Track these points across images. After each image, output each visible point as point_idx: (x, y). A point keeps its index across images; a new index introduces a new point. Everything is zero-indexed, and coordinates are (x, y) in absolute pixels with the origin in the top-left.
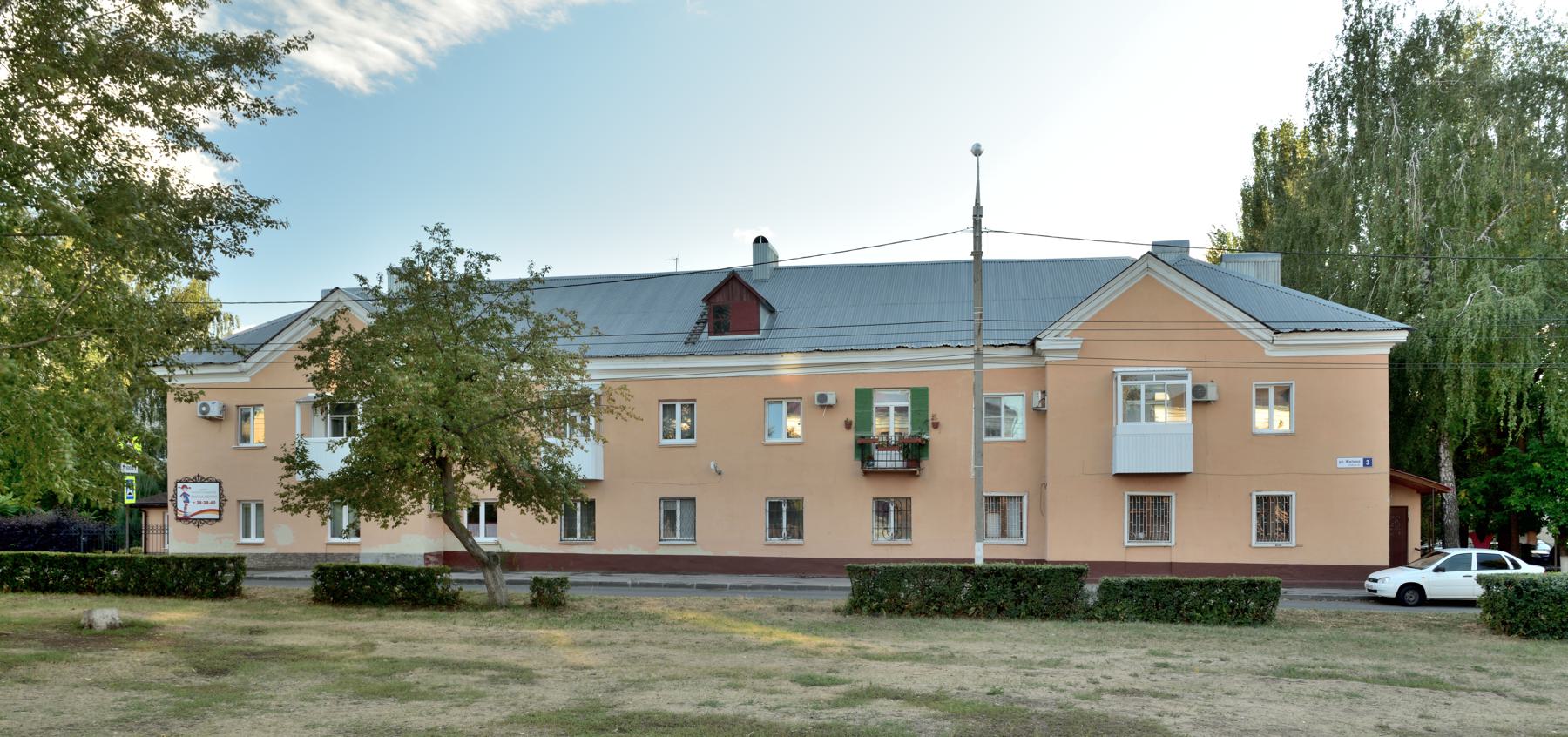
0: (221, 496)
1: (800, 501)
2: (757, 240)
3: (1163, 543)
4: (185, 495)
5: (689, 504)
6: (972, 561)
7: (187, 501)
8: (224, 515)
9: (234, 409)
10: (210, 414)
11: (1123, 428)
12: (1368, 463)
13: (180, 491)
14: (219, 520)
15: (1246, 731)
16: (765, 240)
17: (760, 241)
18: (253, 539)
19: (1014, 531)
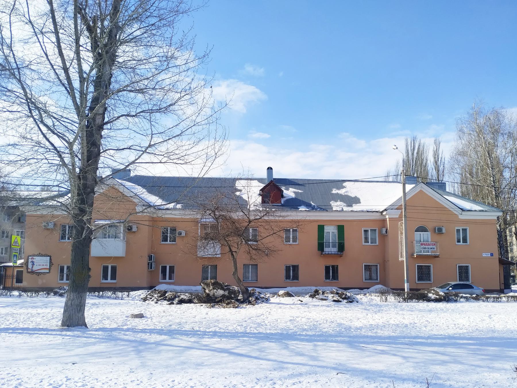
0: (51, 262)
1: (298, 266)
2: (268, 168)
3: (429, 282)
4: (33, 262)
5: (255, 266)
6: (228, 86)
7: (33, 264)
8: (51, 271)
9: (59, 225)
10: (49, 227)
11: (307, 296)
12: (492, 255)
13: (30, 260)
14: (49, 272)
15: (1, 31)
16: (271, 169)
17: (270, 169)
18: (109, 280)
19: (374, 276)
